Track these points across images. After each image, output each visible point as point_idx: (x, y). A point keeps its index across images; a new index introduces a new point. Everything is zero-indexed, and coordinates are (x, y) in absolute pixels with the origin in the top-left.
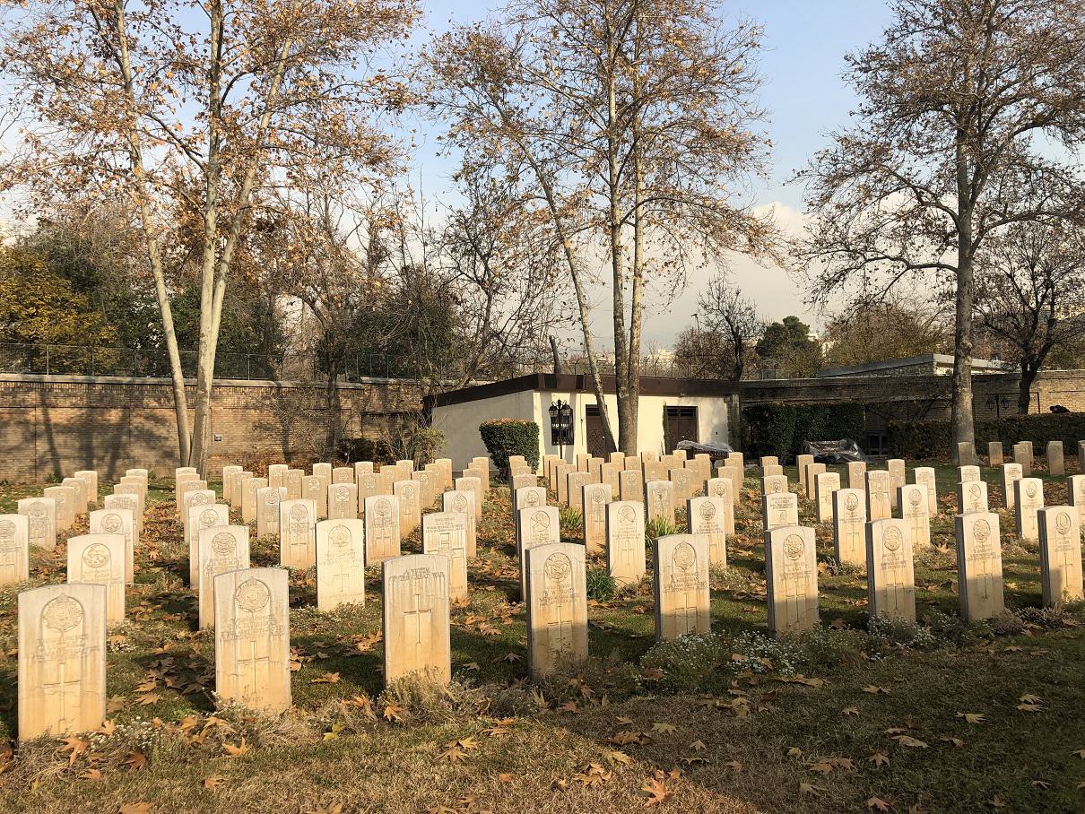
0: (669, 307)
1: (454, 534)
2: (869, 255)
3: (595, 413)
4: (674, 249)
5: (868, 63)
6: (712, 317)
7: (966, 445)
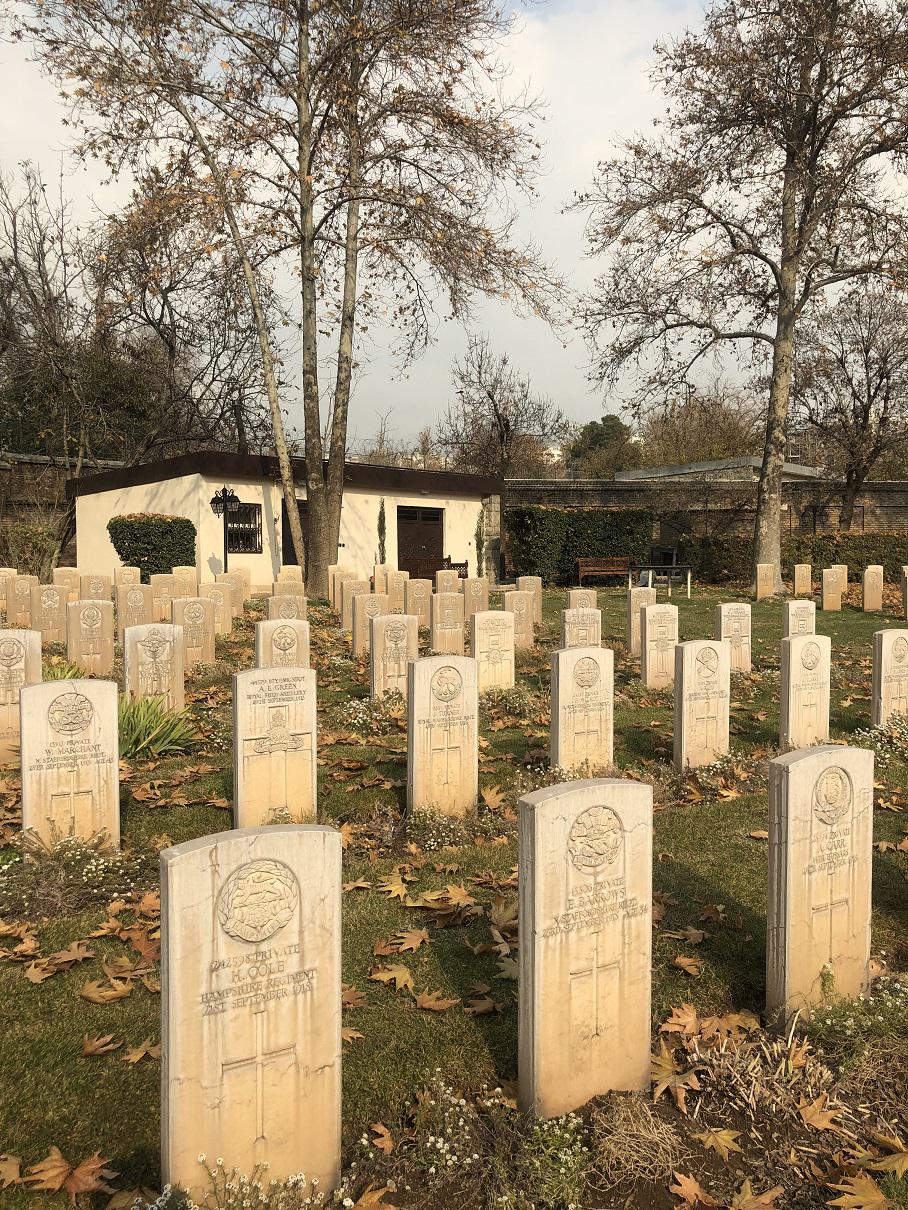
2: (670, 319)
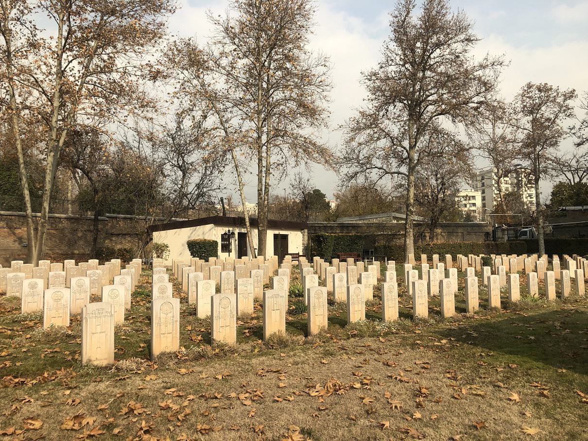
0: (278, 186)
1: (249, 287)
3: (242, 237)
4: (282, 158)
5: (371, 76)
6: (295, 191)
7: (411, 256)
